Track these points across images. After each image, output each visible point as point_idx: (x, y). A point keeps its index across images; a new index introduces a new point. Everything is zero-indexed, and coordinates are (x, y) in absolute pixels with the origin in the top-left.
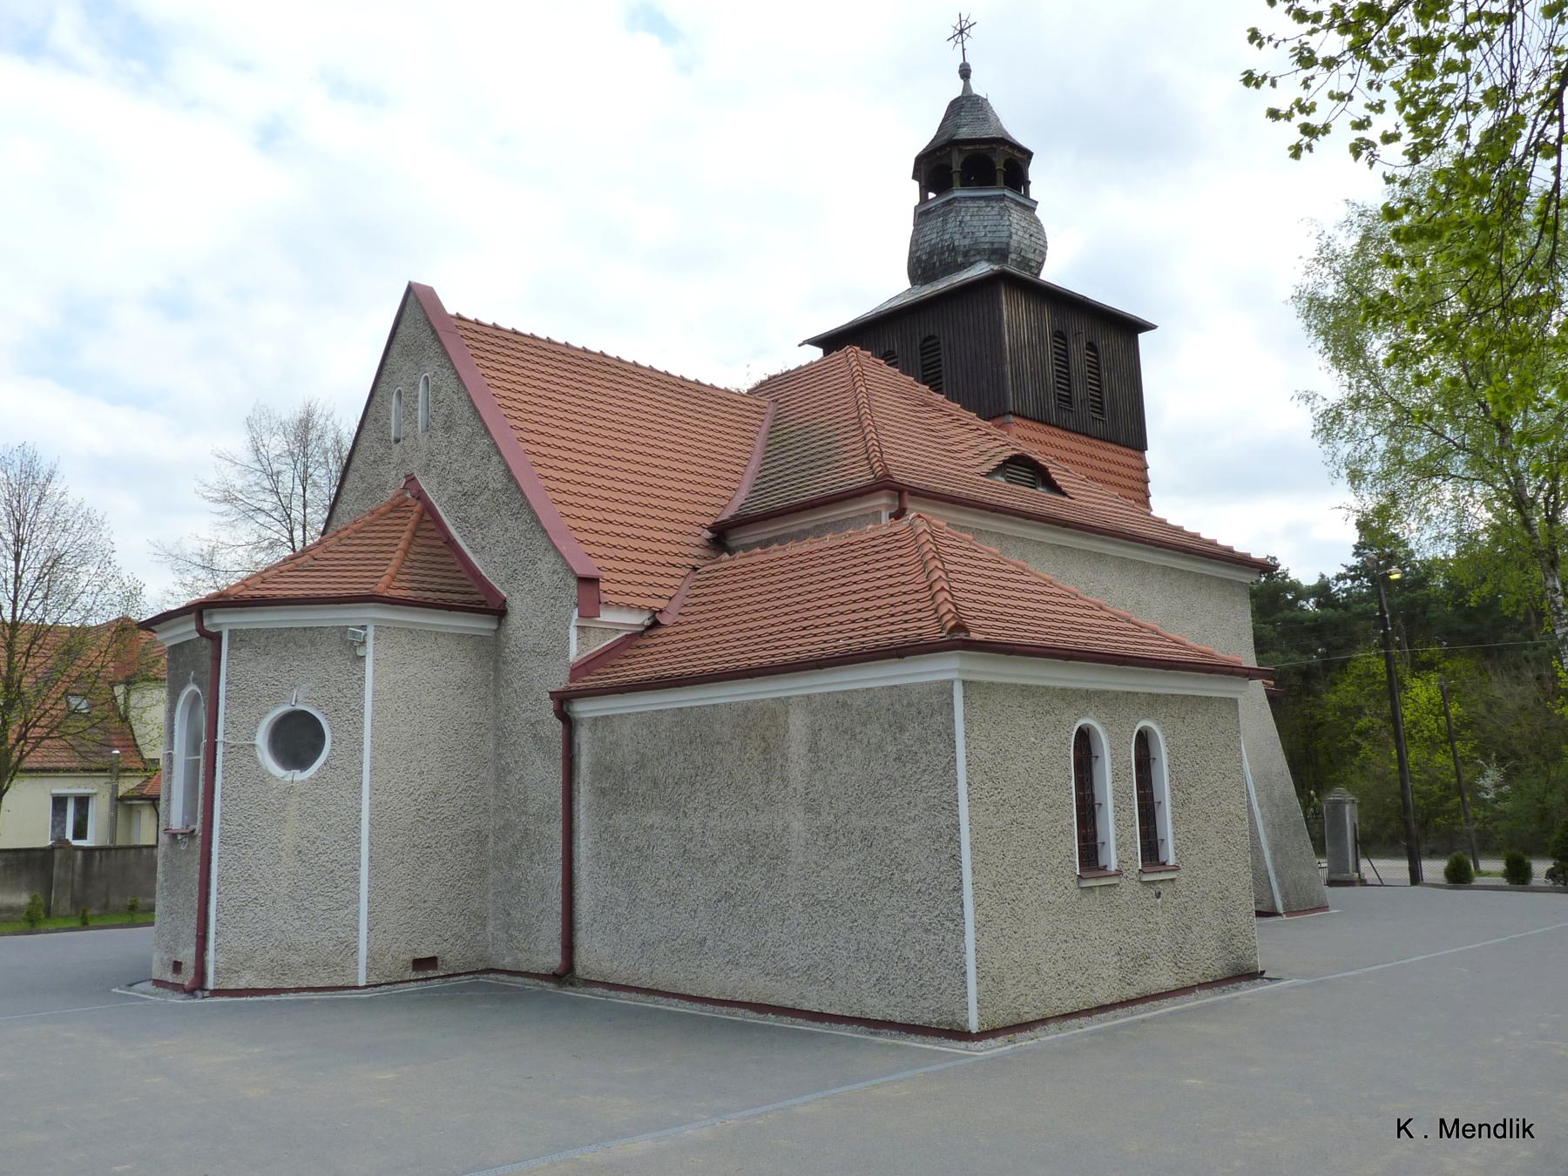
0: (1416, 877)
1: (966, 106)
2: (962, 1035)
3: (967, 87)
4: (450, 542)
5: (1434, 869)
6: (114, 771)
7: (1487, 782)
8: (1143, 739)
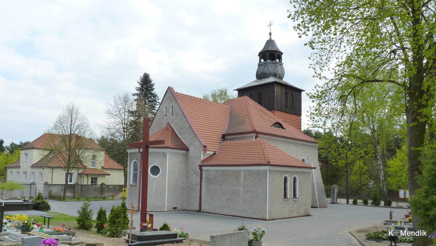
0: (348, 203)
1: (270, 42)
2: (266, 220)
3: (270, 38)
4: (177, 136)
5: (359, 201)
6: (78, 168)
7: (371, 184)
8: (295, 178)
